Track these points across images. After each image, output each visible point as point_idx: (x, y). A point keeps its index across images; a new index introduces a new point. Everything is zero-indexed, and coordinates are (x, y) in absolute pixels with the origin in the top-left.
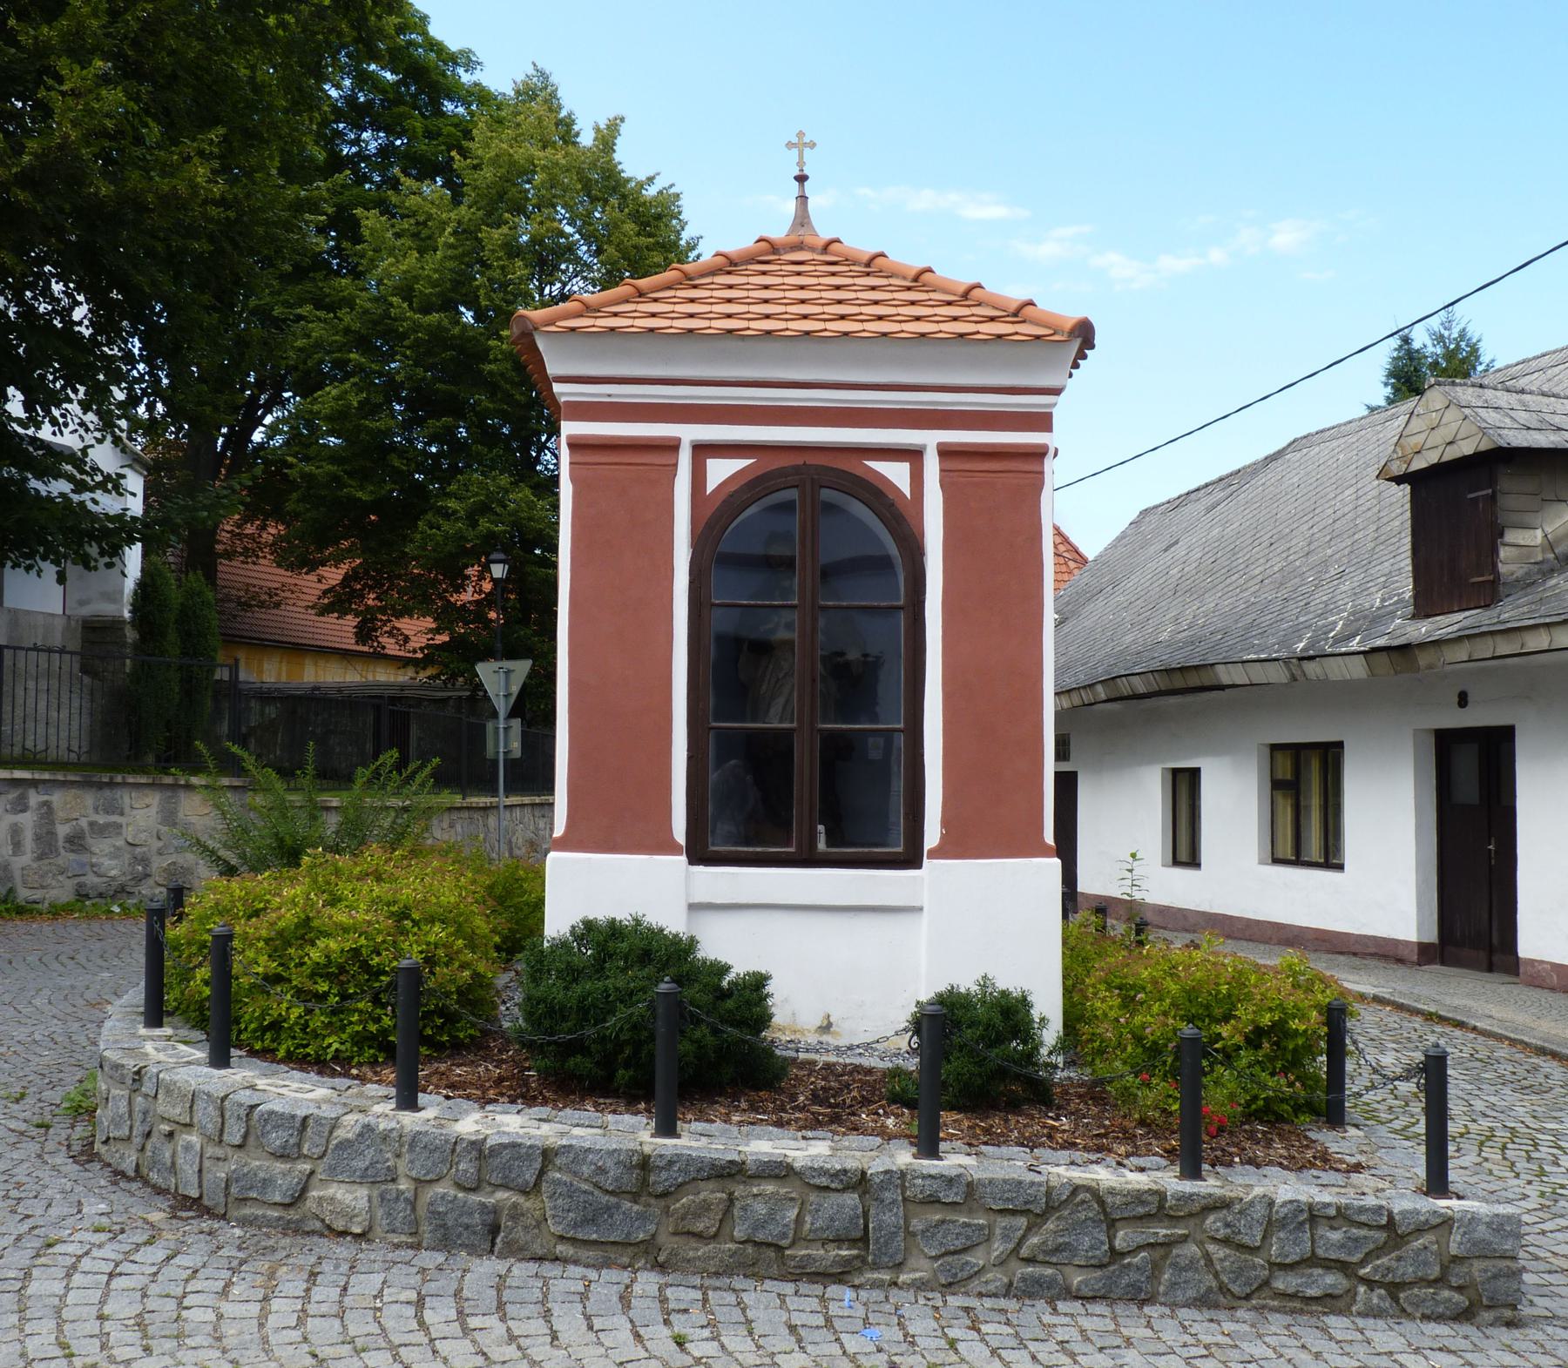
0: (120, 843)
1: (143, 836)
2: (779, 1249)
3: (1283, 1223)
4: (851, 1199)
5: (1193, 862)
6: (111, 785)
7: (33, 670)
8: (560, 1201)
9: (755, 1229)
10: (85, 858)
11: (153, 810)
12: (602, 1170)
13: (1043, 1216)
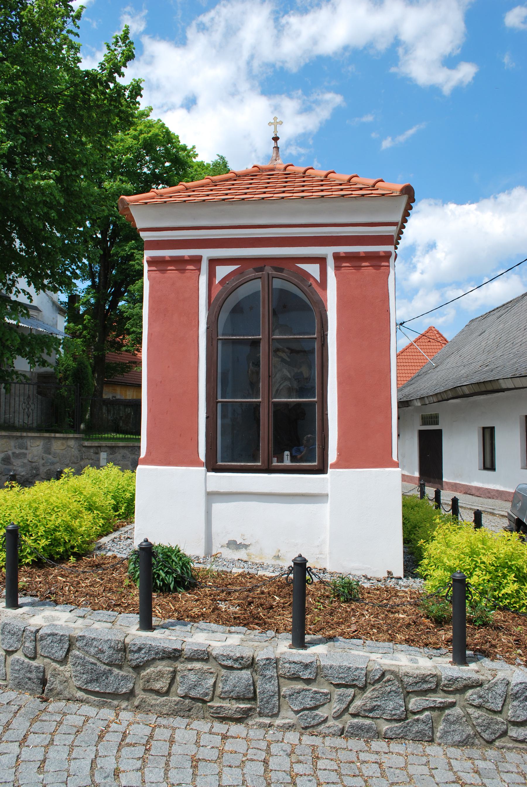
0: (26, 461)
1: (36, 458)
2: (204, 702)
3: (516, 696)
4: (246, 674)
5: (492, 468)
6: (21, 437)
7: (17, 392)
8: (79, 668)
9: (190, 689)
10: (10, 467)
11: (41, 447)
12: (102, 652)
13: (363, 689)
